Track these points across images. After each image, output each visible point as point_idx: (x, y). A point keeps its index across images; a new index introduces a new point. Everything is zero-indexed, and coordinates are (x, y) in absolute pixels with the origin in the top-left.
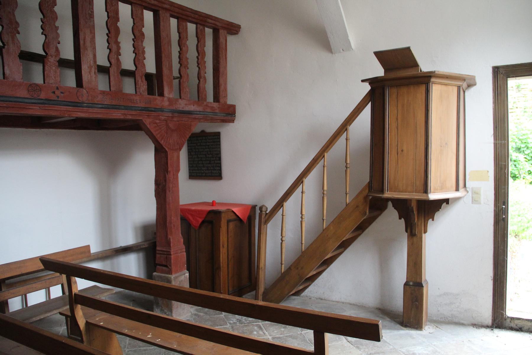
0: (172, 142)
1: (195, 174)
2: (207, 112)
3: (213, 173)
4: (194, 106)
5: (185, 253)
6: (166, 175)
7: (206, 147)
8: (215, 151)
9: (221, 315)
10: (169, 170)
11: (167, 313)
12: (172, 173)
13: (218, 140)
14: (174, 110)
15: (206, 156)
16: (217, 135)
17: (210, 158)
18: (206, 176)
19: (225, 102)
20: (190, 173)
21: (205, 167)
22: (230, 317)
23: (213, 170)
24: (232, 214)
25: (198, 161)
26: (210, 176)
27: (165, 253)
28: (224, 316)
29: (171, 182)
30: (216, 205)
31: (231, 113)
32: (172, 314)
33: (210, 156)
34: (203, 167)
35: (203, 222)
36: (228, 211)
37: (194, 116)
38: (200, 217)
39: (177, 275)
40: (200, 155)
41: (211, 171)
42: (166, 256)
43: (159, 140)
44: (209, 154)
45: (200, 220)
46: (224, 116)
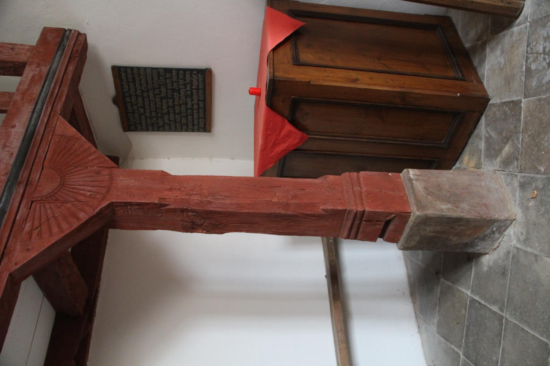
0: (89, 188)
1: (200, 121)
2: (40, 94)
3: (198, 86)
4: (14, 126)
5: (362, 173)
6: (170, 209)
7: (145, 95)
8: (152, 79)
9: (522, 105)
10: (156, 202)
11: (494, 229)
12: (167, 194)
13: (129, 71)
14: (8, 180)
15: (164, 98)
16: (117, 70)
17: (167, 89)
18: (204, 101)
19: (28, 50)
20: (198, 131)
21: (186, 102)
22: (534, 84)
23: (192, 85)
24: (281, 51)
25: (175, 113)
26: (204, 93)
27: (357, 222)
28: (525, 97)
29: (186, 197)
30: (260, 87)
31: (59, 40)
32: (500, 221)
33: (163, 89)
34: (186, 104)
35: (294, 122)
36: (271, 62)
37: (41, 129)
38: (282, 129)
39: (412, 200)
40: (162, 110)
41: (194, 91)
42: (365, 221)
43: (76, 224)
44: (161, 92)
45: (289, 127)
46: (62, 55)
